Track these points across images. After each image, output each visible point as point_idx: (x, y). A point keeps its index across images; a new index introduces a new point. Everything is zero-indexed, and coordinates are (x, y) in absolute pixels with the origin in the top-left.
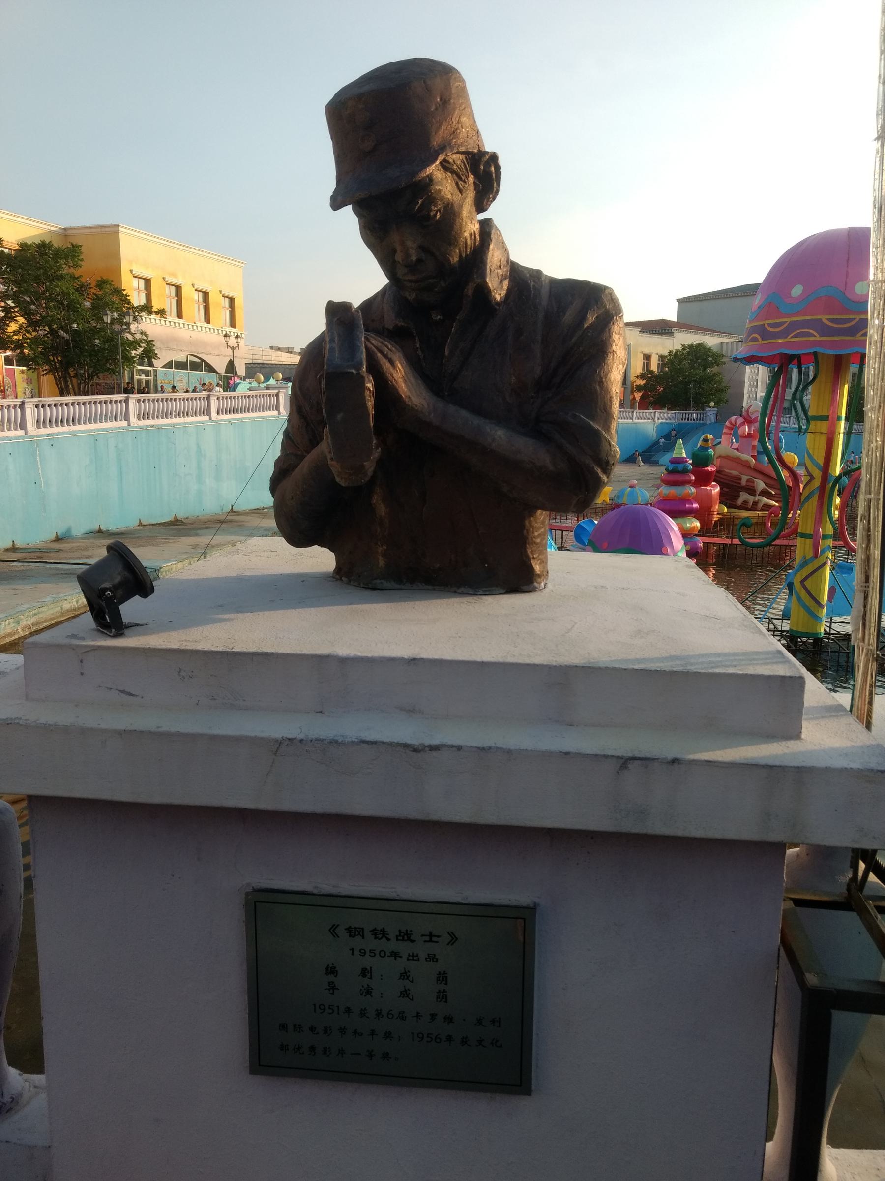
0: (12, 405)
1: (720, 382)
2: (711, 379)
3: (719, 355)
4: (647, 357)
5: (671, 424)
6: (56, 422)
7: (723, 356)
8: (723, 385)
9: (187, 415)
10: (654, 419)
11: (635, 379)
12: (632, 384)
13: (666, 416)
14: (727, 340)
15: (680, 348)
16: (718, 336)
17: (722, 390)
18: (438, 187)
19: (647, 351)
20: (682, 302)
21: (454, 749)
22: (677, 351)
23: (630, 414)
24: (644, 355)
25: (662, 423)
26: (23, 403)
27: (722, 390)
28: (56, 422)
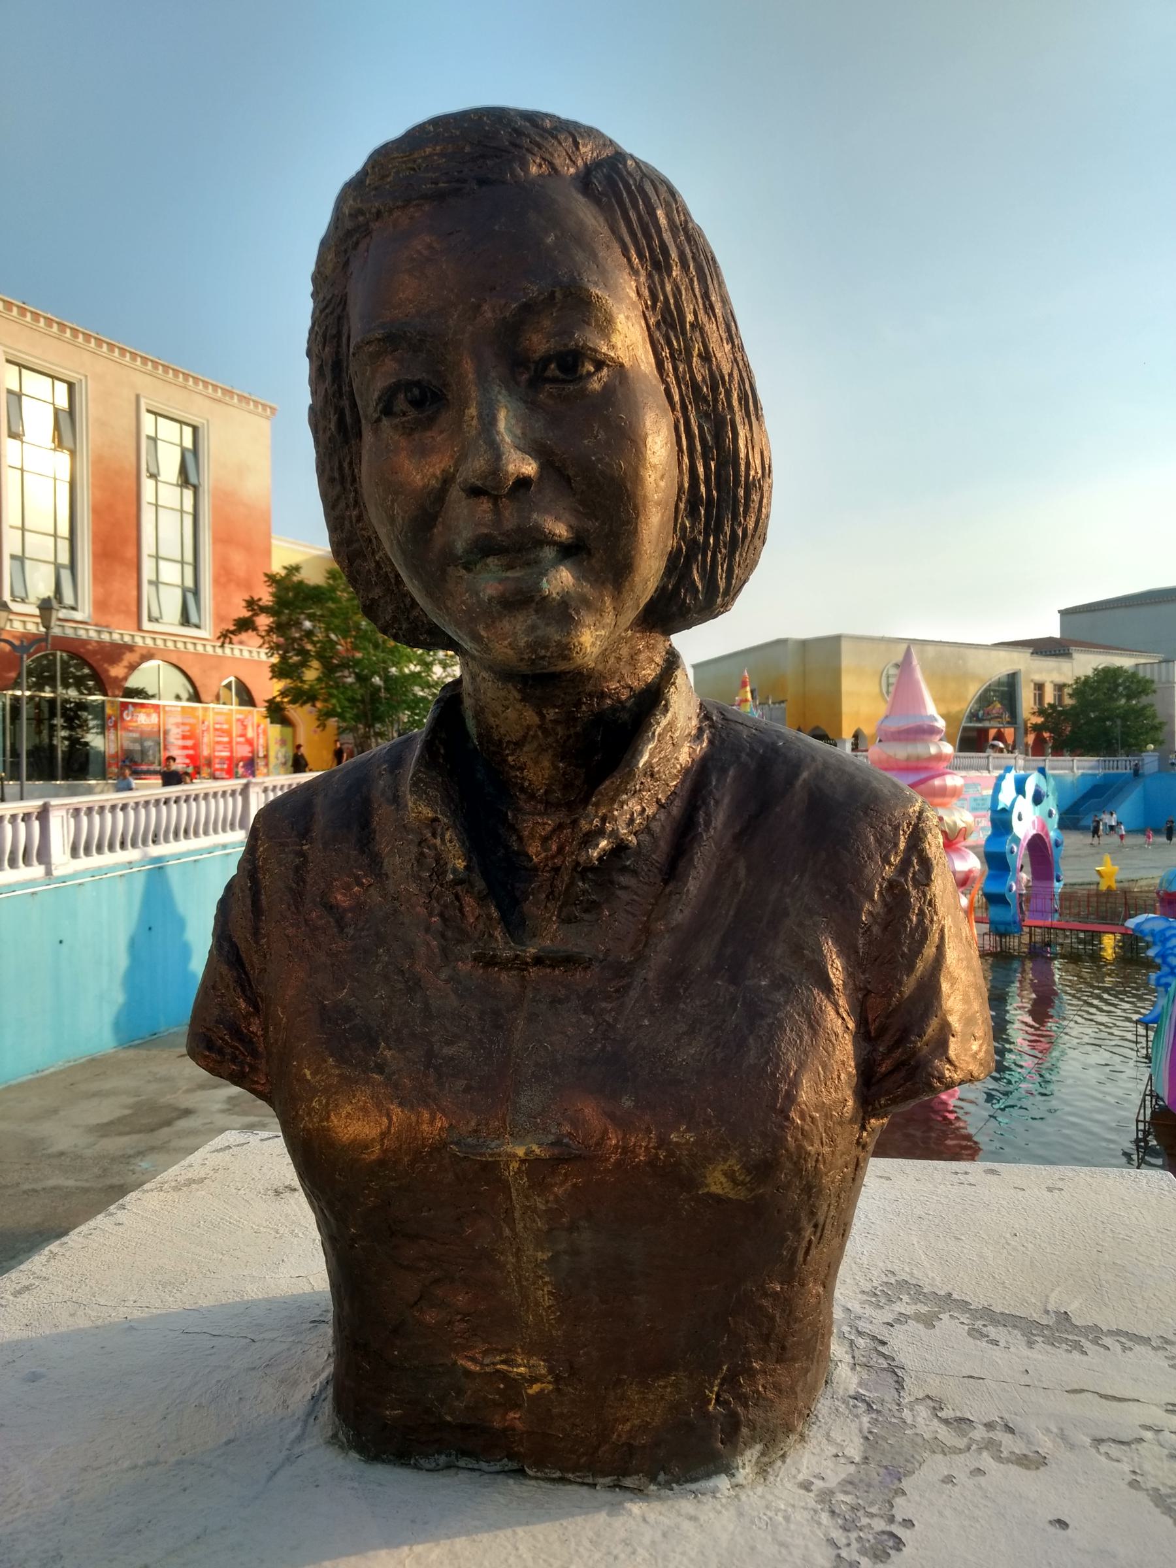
0: (211, 791)
1: (1154, 716)
2: (1140, 713)
3: (1147, 681)
4: (1040, 687)
5: (1095, 775)
6: (186, 832)
7: (1153, 682)
8: (1157, 721)
9: (196, 834)
10: (1072, 769)
11: (1030, 716)
12: (1025, 723)
13: (1086, 764)
14: (1143, 661)
15: (1090, 673)
16: (1131, 656)
17: (1156, 728)
18: (270, 590)
19: (1037, 678)
20: (1064, 613)
21: (895, 1378)
22: (1087, 678)
23: (984, 761)
24: (1055, 685)
25: (1083, 775)
26: (246, 787)
27: (1156, 728)
28: (186, 832)
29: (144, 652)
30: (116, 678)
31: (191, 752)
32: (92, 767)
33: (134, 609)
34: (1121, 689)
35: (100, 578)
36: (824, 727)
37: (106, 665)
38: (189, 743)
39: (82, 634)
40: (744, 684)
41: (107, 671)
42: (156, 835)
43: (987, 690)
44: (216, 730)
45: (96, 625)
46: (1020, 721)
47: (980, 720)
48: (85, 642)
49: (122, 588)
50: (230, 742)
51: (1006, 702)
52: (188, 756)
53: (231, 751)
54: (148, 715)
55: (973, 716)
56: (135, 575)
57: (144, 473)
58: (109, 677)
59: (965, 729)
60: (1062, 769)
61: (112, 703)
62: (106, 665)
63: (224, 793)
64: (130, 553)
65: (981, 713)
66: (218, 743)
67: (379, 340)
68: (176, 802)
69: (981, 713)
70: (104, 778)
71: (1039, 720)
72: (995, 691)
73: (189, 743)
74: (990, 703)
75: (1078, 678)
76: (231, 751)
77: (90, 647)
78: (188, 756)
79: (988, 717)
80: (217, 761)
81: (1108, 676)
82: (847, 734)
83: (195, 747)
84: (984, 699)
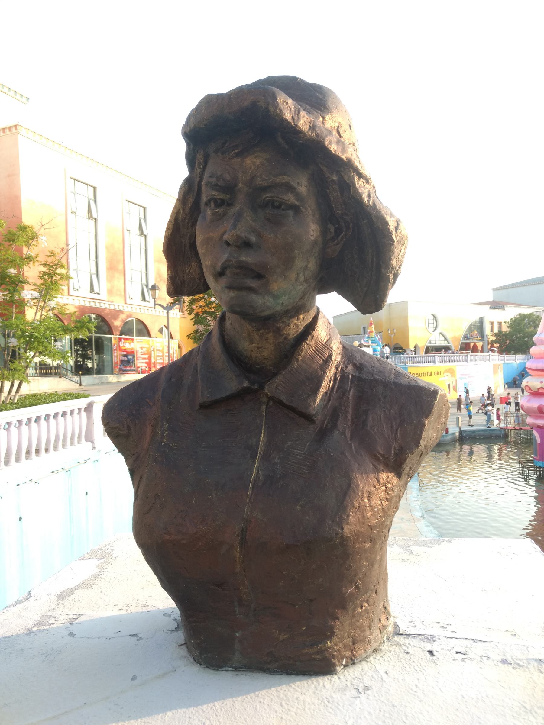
4: (492, 323)
13: (521, 358)
20: (495, 290)
23: (503, 358)
25: (520, 363)
29: (128, 314)
30: (117, 326)
31: (147, 361)
32: (107, 369)
33: (123, 294)
34: (531, 323)
35: (110, 279)
36: (400, 343)
37: (113, 320)
38: (146, 356)
39: (103, 306)
40: (371, 324)
41: (113, 323)
42: (28, 452)
43: (471, 325)
44: (157, 350)
45: (108, 301)
46: (485, 338)
47: (468, 339)
48: (104, 310)
49: (119, 283)
50: (163, 356)
51: (479, 330)
52: (146, 363)
53: (163, 360)
54: (130, 343)
55: (465, 337)
56: (123, 278)
57: (125, 230)
58: (114, 326)
59: (462, 343)
60: (511, 360)
61: (115, 338)
62: (113, 320)
63: (72, 412)
64: (121, 267)
65: (468, 336)
66: (158, 356)
67: (220, 187)
68: (54, 417)
69: (468, 336)
70: (112, 374)
71: (494, 338)
72: (474, 325)
73: (146, 356)
74: (472, 331)
75: (512, 319)
76: (163, 360)
77: (106, 312)
78: (146, 363)
79: (472, 337)
80: (158, 364)
81: (523, 317)
82: (412, 347)
83: (149, 358)
84: (470, 329)
